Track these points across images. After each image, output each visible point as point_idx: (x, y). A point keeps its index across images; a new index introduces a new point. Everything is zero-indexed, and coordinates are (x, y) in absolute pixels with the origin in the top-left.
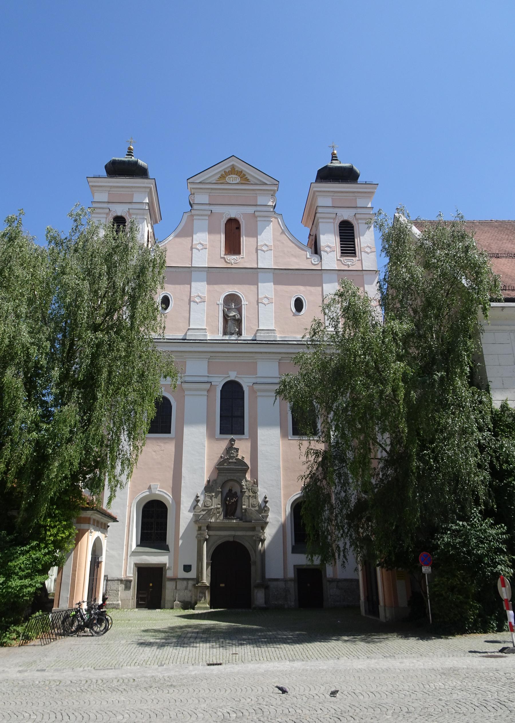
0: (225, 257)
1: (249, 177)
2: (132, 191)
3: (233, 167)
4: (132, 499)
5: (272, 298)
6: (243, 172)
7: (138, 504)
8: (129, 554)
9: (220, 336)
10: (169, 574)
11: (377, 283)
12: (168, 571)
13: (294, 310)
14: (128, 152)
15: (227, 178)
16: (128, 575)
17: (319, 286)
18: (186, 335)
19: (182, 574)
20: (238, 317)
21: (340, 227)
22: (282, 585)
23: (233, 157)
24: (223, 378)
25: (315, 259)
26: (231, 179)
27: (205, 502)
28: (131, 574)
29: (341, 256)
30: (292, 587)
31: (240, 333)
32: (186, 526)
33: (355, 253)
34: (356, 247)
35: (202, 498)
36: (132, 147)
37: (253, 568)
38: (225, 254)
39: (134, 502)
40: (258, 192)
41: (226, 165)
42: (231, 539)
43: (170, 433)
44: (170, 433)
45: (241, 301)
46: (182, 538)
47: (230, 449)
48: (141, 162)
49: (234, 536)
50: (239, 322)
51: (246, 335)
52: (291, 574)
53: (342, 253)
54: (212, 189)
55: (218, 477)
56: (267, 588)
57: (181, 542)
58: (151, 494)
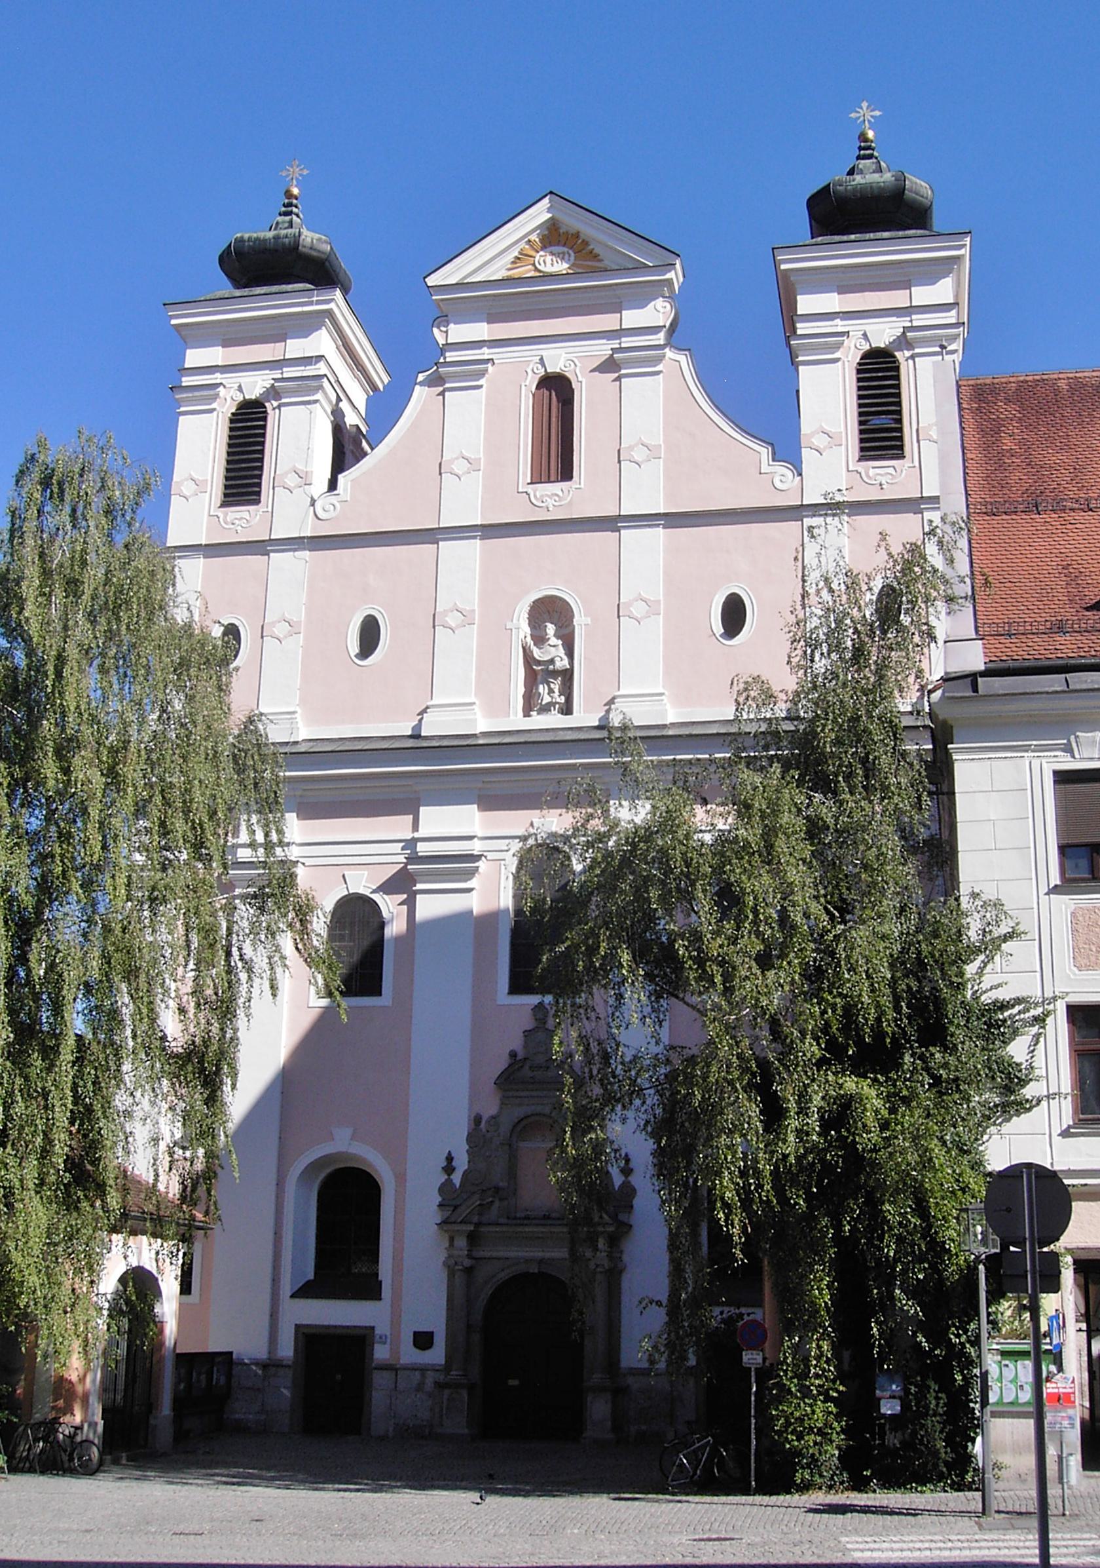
5: (658, 602)
6: (582, 236)
8: (286, 1289)
9: (515, 720)
10: (381, 1353)
11: (612, 349)
12: (376, 1346)
13: (719, 629)
18: (418, 726)
19: (410, 1355)
20: (562, 663)
21: (859, 371)
25: (782, 473)
29: (860, 460)
30: (798, 291)
31: (567, 710)
33: (901, 448)
34: (264, 477)
42: (534, 1269)
43: (380, 994)
44: (380, 994)
45: (573, 616)
48: (309, 237)
49: (541, 1261)
51: (585, 716)
53: (862, 449)
55: (501, 1108)
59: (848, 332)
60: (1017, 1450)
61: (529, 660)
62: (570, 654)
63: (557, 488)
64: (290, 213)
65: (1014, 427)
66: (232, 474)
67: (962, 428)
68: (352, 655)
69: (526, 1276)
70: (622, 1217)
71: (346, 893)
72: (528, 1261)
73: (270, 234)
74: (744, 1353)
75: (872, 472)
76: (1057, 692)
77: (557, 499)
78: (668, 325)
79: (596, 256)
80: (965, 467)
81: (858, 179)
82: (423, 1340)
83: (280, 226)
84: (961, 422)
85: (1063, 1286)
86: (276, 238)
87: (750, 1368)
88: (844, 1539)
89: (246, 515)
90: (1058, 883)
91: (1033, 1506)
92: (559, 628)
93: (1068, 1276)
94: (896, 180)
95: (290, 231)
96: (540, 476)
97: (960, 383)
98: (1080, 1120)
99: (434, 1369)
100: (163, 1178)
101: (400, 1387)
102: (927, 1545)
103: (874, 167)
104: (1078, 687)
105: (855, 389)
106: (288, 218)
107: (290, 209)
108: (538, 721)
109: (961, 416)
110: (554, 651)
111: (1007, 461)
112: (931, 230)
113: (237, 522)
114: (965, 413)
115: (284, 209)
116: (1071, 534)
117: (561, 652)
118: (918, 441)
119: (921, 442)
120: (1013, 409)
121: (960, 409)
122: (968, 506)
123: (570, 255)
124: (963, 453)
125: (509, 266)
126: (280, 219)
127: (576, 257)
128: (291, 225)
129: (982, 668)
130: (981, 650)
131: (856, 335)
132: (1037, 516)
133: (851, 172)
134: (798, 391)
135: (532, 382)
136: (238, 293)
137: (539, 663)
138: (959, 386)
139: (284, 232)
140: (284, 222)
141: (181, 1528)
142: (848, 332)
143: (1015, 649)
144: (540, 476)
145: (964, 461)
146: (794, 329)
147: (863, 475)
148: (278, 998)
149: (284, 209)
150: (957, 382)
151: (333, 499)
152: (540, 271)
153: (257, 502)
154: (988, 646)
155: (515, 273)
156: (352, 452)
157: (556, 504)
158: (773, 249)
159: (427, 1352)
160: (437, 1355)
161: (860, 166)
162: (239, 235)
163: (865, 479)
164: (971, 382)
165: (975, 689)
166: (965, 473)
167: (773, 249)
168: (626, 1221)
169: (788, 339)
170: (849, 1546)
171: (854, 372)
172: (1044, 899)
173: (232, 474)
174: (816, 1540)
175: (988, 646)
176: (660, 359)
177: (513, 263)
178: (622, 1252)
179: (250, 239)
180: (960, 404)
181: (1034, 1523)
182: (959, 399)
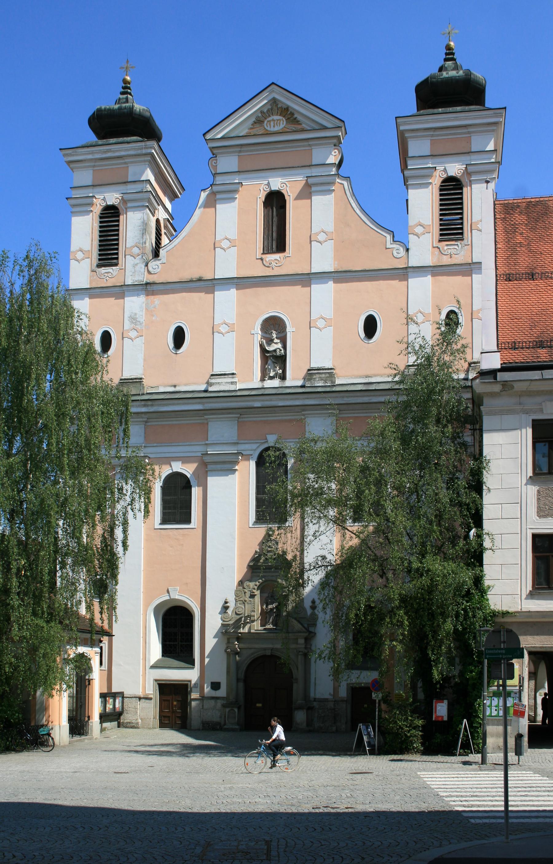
0: (264, 256)
1: (299, 118)
2: (125, 163)
3: (274, 101)
4: (146, 606)
6: (290, 110)
7: (156, 610)
9: (256, 383)
13: (362, 335)
14: (123, 88)
15: (266, 122)
16: (147, 692)
17: (404, 281)
21: (441, 190)
22: (331, 705)
23: (273, 86)
24: (258, 445)
26: (272, 123)
27: (236, 608)
28: (151, 690)
31: (283, 377)
32: (187, 737)
35: (232, 605)
36: (128, 78)
37: (295, 686)
38: (263, 253)
39: (149, 609)
40: (311, 143)
41: (261, 103)
42: (268, 653)
46: (207, 657)
47: (268, 537)
48: (138, 107)
49: (272, 649)
50: (281, 360)
52: (343, 693)
54: (242, 145)
56: (310, 709)
57: (207, 660)
58: (171, 600)
59: (436, 167)
60: (497, 735)
61: (263, 351)
62: (285, 347)
63: (277, 256)
64: (127, 93)
65: (522, 229)
66: (103, 248)
67: (495, 230)
68: (171, 349)
69: (264, 657)
70: (311, 629)
71: (171, 472)
72: (265, 649)
73: (117, 107)
74: (373, 694)
75: (446, 248)
76: (536, 380)
77: (277, 262)
78: (337, 163)
79: (298, 121)
80: (496, 253)
81: (445, 74)
82: (215, 686)
83: (121, 101)
84: (495, 226)
85: (543, 520)
86: (120, 109)
87: (376, 700)
88: (419, 773)
89: (111, 271)
90: (531, 475)
91: (502, 762)
92: (278, 333)
93: (526, 653)
94: (465, 75)
95: (127, 105)
96: (267, 250)
97: (496, 202)
98: (536, 588)
99: (223, 698)
100: (97, 616)
101: (205, 707)
102: (456, 776)
103: (453, 66)
104: (547, 377)
105: (438, 210)
106: (125, 96)
107: (126, 90)
108: (269, 383)
109: (495, 223)
110: (276, 346)
111: (518, 249)
112: (484, 105)
113: (106, 274)
114: (499, 222)
115: (123, 90)
116: (549, 292)
117: (280, 346)
118: (471, 230)
119: (473, 231)
120: (524, 218)
121: (495, 219)
122: (496, 275)
123: (283, 121)
124: (496, 245)
125: (251, 126)
126: (121, 96)
127: (286, 122)
128: (127, 101)
129: (499, 366)
130: (499, 357)
131: (440, 168)
132: (532, 281)
133: (441, 69)
134: (407, 200)
135: (262, 196)
136: (100, 142)
137: (268, 352)
138: (495, 205)
139: (124, 105)
140: (123, 99)
141: (117, 770)
142: (436, 167)
143: (516, 356)
144: (267, 250)
145: (496, 249)
146: (406, 166)
147: (441, 249)
148: (461, 765)
149: (123, 90)
150: (494, 202)
151: (158, 263)
152: (267, 130)
153: (116, 265)
154: (503, 355)
155: (253, 132)
156: (165, 233)
157: (276, 265)
158: (396, 118)
159: (217, 692)
160: (222, 692)
161: (446, 65)
162: (99, 107)
163: (442, 252)
164: (501, 202)
165: (495, 378)
166: (496, 257)
167: (396, 118)
168: (313, 631)
169: (402, 171)
170: (422, 776)
171: (438, 190)
172: (524, 487)
173: (103, 248)
174: (407, 773)
175: (503, 355)
176: (333, 183)
177: (252, 125)
178: (311, 645)
179: (105, 109)
180: (495, 215)
181: (502, 767)
182: (495, 212)
